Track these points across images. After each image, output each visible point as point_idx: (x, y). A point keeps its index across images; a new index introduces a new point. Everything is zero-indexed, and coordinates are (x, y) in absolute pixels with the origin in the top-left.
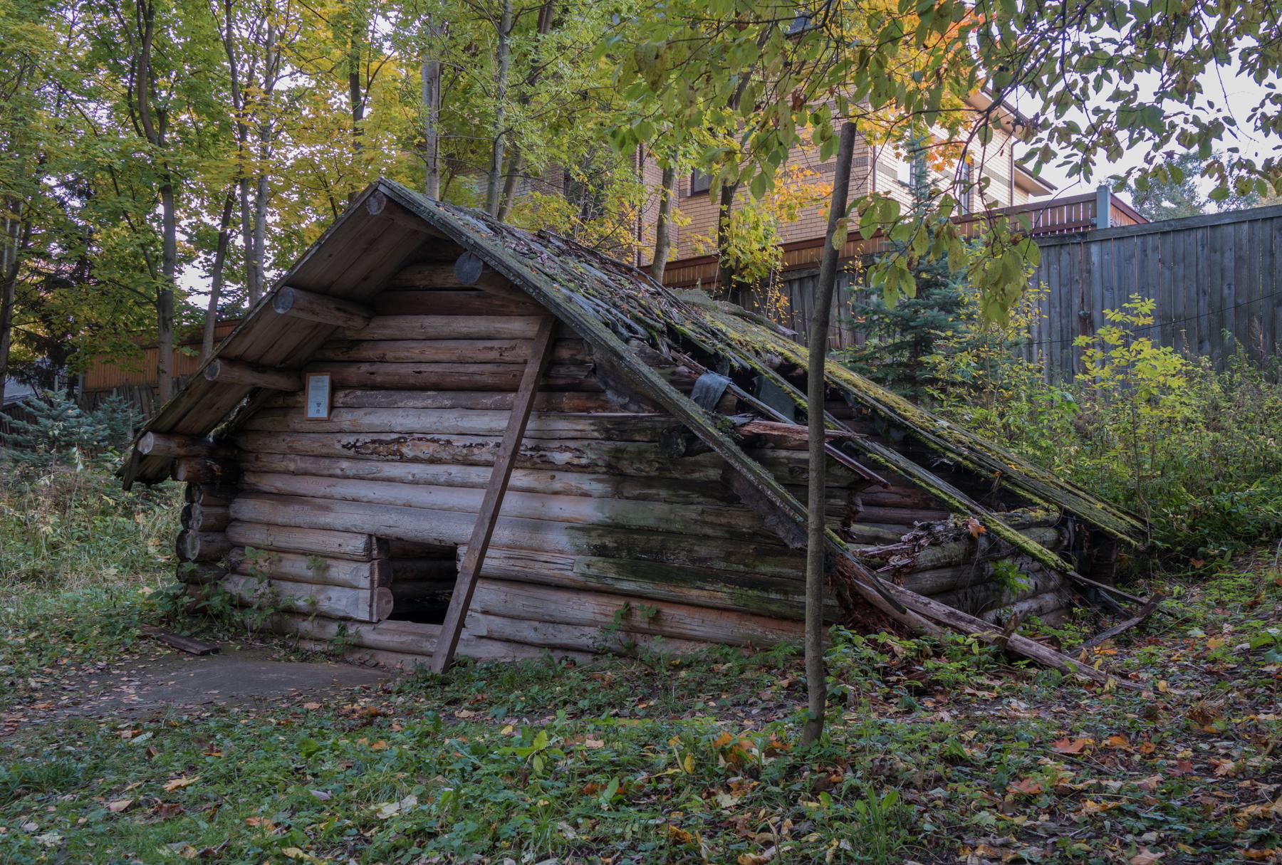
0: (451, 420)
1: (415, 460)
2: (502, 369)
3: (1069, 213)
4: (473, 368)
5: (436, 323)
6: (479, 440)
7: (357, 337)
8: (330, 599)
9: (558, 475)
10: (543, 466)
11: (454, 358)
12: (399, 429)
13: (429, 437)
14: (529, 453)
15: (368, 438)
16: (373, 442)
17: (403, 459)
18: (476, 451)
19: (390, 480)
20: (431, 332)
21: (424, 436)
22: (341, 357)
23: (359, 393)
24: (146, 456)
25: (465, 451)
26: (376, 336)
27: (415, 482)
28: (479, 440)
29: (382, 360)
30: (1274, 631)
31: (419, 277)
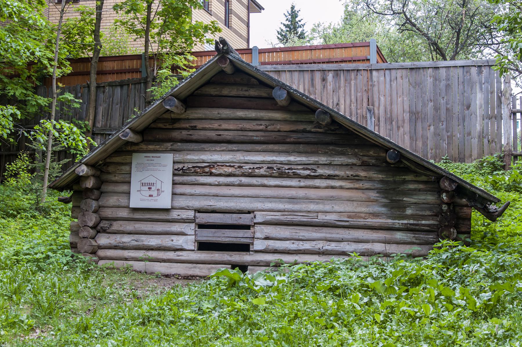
0: (240, 157)
1: (220, 175)
2: (267, 134)
3: (265, 58)
4: (251, 134)
5: (215, 112)
6: (258, 166)
7: (178, 117)
8: (172, 240)
9: (302, 180)
10: (294, 176)
11: (238, 128)
12: (209, 161)
13: (228, 164)
14: (287, 171)
15: (190, 166)
16: (193, 167)
17: (211, 174)
18: (256, 171)
19: (210, 185)
20: (223, 116)
21: (223, 164)
22: (168, 127)
23: (179, 144)
24: (81, 176)
25: (250, 171)
26: (190, 117)
27: (219, 185)
28: (258, 166)
29: (194, 128)
30: (3, 333)
31: (212, 91)
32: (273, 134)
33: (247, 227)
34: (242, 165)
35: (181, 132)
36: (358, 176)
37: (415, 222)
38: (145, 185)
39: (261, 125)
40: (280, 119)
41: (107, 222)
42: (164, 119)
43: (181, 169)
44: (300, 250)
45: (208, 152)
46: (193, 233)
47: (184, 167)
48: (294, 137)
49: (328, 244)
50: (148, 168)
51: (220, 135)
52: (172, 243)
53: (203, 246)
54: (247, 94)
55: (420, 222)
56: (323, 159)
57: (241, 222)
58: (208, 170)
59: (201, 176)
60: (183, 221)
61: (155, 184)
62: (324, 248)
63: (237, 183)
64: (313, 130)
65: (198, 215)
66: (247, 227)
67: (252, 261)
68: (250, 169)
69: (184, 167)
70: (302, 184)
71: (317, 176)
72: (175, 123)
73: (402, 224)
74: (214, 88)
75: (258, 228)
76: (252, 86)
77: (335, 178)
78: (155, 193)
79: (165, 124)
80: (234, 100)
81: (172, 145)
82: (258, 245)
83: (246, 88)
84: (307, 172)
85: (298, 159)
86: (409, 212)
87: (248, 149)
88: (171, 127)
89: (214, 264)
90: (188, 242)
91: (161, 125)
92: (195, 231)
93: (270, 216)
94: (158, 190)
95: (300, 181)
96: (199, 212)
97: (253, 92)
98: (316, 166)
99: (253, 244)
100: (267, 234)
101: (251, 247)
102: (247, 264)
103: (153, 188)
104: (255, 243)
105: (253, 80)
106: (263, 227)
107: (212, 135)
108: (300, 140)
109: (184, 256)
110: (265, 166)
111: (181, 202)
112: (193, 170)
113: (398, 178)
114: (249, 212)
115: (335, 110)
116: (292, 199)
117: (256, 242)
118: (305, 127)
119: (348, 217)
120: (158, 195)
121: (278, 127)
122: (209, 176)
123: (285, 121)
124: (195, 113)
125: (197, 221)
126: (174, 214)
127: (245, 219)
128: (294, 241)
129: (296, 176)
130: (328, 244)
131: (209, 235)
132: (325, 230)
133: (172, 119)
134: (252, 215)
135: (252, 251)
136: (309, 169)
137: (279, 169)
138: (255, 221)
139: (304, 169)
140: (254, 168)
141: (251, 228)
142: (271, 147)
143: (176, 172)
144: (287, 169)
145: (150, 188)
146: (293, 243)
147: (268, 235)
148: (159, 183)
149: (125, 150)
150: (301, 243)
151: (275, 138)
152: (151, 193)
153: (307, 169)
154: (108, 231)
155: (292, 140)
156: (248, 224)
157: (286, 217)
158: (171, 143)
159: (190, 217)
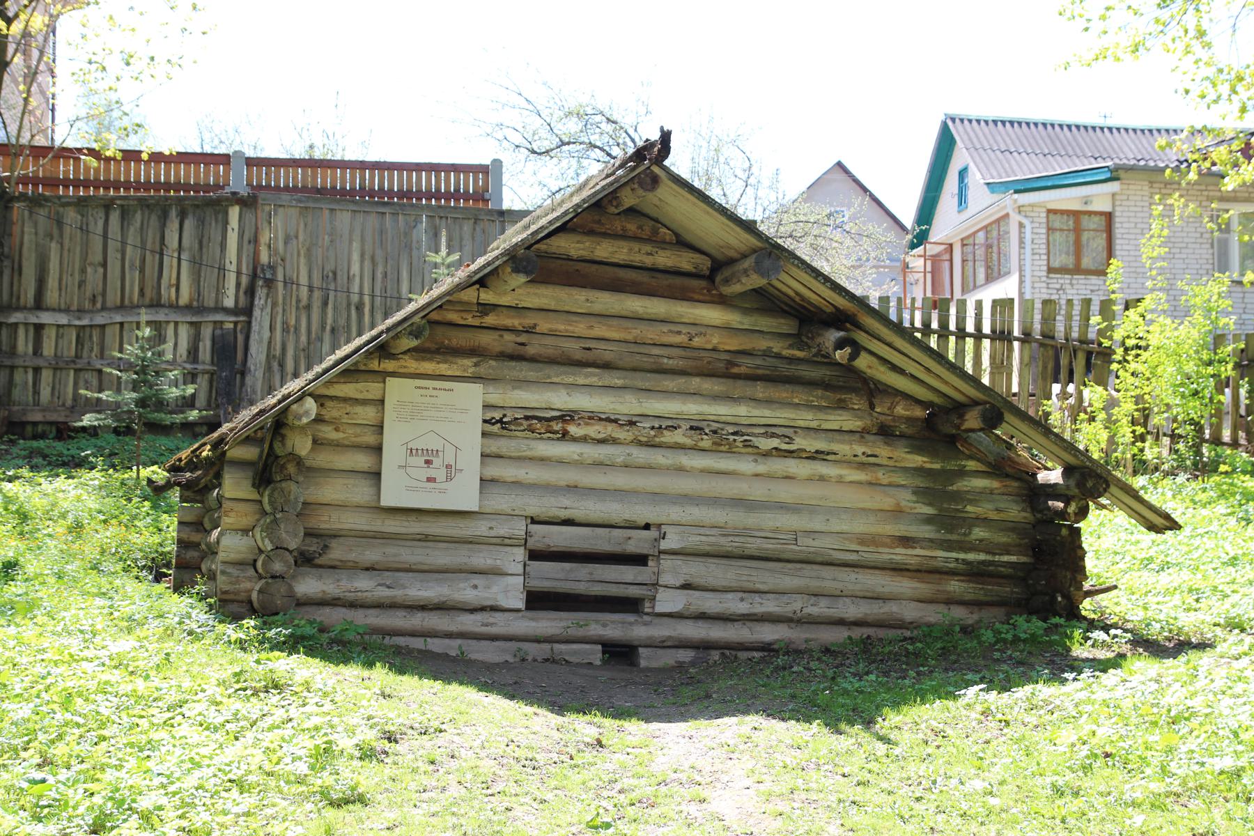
14: (731, 438)
16: (527, 418)
22: (470, 321)
28: (670, 423)
32: (703, 354)
33: (639, 560)
34: (634, 419)
35: (501, 336)
36: (875, 456)
37: (989, 558)
38: (417, 455)
39: (679, 333)
40: (717, 322)
41: (315, 540)
42: (461, 302)
43: (497, 422)
44: (755, 615)
45: (466, 365)
46: (521, 571)
47: (505, 416)
48: (745, 365)
49: (811, 602)
50: (425, 413)
51: (589, 349)
52: (475, 592)
53: (538, 600)
54: (648, 261)
55: (997, 558)
56: (806, 418)
57: (632, 548)
58: (558, 425)
59: (541, 439)
60: (498, 541)
61: (441, 454)
62: (805, 611)
63: (620, 460)
64: (785, 352)
65: (534, 528)
66: (639, 560)
67: (650, 638)
68: (653, 428)
69: (505, 416)
70: (761, 468)
71: (792, 452)
72: (487, 314)
73: (957, 560)
74: (578, 242)
75: (667, 563)
76: (662, 244)
77: (829, 457)
78: (440, 474)
79: (465, 315)
80: (622, 273)
81: (476, 365)
82: (668, 602)
83: (648, 248)
84: (775, 443)
85: (756, 412)
86: (979, 533)
87: (647, 385)
88: (476, 322)
89: (587, 643)
90: (511, 593)
91: (453, 317)
92: (525, 565)
93: (694, 540)
94: (448, 467)
95: (756, 461)
96: (534, 521)
97: (664, 259)
98: (792, 430)
99: (653, 599)
100: (688, 577)
101: (647, 604)
102: (636, 643)
103: (437, 462)
104: (658, 597)
105: (664, 230)
106: (679, 562)
107: (573, 348)
108: (760, 372)
109: (500, 624)
110: (685, 425)
111: (501, 501)
112: (525, 423)
113: (952, 465)
114: (647, 527)
115: (1067, 436)
116: (738, 502)
117: (662, 595)
118: (771, 344)
119: (860, 544)
120: (449, 478)
121: (715, 341)
122: (558, 439)
123: (727, 329)
124: (535, 294)
125: (532, 543)
126: (480, 528)
127: (637, 543)
128: (744, 595)
129: (750, 450)
130: (811, 602)
131: (552, 576)
132: (809, 570)
133: (479, 304)
134: (653, 533)
135: (647, 614)
136: (778, 436)
137: (715, 432)
138: (664, 545)
139: (766, 435)
140: (660, 427)
141: (650, 563)
142: (696, 383)
143: (489, 428)
144: (733, 434)
145: (428, 462)
146: (742, 600)
147: (691, 580)
148: (450, 451)
149: (363, 368)
150: (757, 598)
151: (709, 363)
152: (431, 473)
153: (773, 435)
154: (318, 561)
155: (743, 370)
156: (645, 552)
157: (731, 538)
158: (474, 360)
159: (516, 532)
